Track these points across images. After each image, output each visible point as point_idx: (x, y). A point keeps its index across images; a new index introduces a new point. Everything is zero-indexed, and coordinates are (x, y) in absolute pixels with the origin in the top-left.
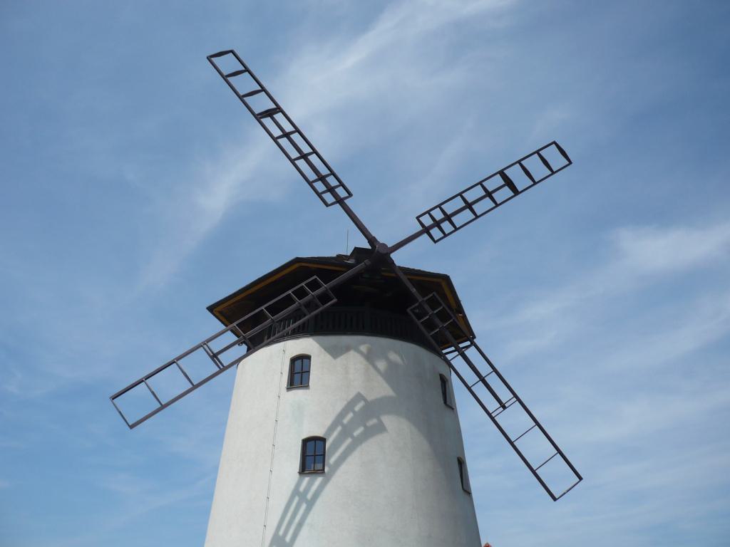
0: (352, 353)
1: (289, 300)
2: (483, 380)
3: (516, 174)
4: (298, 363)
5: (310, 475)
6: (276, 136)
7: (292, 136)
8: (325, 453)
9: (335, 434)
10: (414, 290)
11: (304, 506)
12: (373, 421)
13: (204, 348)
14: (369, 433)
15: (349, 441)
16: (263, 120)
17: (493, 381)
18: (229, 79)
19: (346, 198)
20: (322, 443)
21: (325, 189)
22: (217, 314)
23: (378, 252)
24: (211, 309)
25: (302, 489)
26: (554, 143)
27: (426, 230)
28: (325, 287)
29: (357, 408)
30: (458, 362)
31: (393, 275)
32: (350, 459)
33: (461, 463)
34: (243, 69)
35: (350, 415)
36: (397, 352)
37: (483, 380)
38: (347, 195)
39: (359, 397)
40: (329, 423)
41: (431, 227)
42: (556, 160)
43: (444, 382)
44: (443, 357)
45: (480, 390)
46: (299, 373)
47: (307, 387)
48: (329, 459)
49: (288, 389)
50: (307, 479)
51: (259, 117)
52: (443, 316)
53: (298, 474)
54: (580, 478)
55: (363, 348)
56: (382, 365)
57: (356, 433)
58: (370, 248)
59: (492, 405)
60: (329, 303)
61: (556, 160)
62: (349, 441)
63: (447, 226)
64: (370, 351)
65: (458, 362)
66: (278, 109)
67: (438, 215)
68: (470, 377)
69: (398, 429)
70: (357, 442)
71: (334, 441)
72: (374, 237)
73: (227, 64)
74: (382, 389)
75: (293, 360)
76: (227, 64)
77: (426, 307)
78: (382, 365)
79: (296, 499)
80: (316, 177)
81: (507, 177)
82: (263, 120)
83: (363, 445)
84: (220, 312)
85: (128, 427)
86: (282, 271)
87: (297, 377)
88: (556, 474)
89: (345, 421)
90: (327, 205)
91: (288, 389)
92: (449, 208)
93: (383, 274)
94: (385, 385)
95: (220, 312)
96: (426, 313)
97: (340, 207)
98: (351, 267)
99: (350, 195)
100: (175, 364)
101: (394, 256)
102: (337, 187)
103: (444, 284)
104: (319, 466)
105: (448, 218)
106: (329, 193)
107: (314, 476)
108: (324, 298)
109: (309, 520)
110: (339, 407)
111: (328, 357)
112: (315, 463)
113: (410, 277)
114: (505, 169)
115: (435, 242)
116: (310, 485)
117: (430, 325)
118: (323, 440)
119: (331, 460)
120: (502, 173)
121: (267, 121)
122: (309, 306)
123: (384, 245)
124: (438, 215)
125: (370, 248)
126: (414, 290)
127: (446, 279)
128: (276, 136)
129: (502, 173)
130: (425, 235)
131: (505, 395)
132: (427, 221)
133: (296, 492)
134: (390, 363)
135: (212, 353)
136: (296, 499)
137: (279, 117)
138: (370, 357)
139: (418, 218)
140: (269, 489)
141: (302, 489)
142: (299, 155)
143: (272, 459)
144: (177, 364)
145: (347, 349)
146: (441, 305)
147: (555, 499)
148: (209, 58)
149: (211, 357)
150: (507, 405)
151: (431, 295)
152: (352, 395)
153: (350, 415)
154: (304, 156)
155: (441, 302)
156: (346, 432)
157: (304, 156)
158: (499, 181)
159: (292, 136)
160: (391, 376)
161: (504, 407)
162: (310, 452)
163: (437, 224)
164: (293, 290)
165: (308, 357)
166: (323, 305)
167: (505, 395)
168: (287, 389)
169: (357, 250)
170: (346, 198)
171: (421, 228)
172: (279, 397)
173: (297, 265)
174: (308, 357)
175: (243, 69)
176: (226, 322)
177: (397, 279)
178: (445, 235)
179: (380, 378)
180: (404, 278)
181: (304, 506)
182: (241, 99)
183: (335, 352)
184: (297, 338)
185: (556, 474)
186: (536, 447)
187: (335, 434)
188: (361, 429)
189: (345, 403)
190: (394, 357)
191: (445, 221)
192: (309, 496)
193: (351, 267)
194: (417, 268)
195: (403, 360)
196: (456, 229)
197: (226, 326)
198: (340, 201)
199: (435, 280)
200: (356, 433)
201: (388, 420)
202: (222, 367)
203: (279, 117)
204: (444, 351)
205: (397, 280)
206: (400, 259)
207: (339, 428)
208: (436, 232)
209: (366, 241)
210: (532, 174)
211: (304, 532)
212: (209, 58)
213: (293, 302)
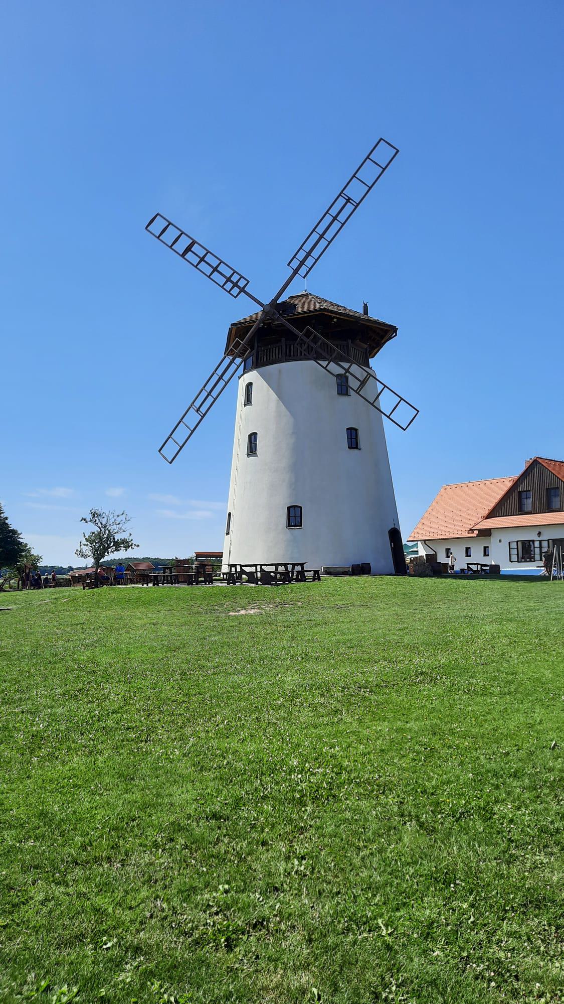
17: (210, 400)
27: (242, 290)
58: (278, 302)
59: (197, 404)
63: (235, 278)
67: (229, 286)
81: (185, 251)
85: (160, 213)
88: (169, 451)
105: (229, 280)
114: (179, 254)
120: (183, 255)
124: (229, 286)
125: (278, 302)
129: (183, 255)
131: (204, 410)
132: (236, 291)
135: (360, 386)
158: (189, 255)
161: (349, 199)
163: (235, 285)
167: (204, 410)
185: (169, 451)
186: (181, 434)
196: (235, 272)
198: (296, 272)
208: (242, 283)
210: (164, 227)
213: (324, 343)
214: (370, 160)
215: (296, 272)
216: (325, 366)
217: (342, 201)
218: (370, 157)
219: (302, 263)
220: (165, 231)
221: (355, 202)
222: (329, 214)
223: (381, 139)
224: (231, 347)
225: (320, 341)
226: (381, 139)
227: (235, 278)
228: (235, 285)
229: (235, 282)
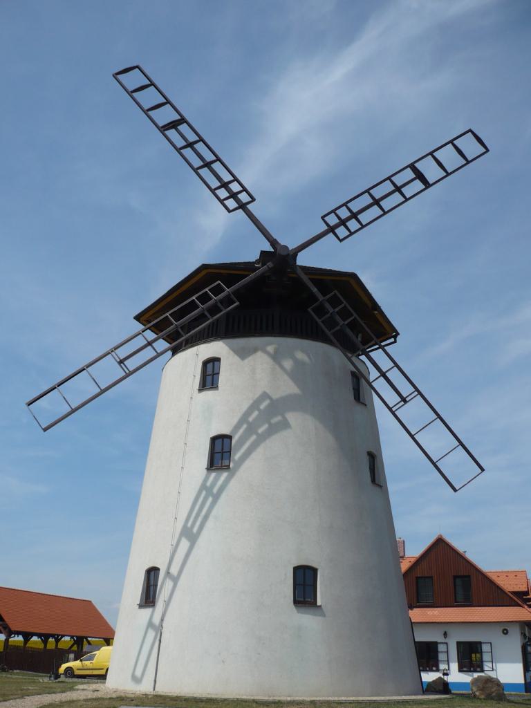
0: (259, 354)
1: (193, 306)
2: (383, 375)
4: (210, 366)
5: (216, 471)
6: (222, 197)
7: (213, 166)
8: (231, 449)
9: (241, 431)
10: (315, 290)
11: (210, 499)
12: (275, 420)
14: (272, 430)
15: (254, 437)
16: (167, 132)
17: (394, 375)
18: (150, 113)
20: (229, 440)
25: (208, 484)
26: (470, 131)
27: (332, 229)
29: (262, 407)
31: (294, 275)
32: (254, 455)
34: (165, 101)
35: (256, 413)
36: (303, 351)
37: (383, 375)
38: (250, 199)
39: (265, 396)
40: (235, 421)
41: (337, 226)
42: (470, 147)
46: (209, 376)
47: (217, 388)
48: (235, 454)
49: (200, 390)
50: (213, 475)
51: (164, 129)
53: (205, 471)
55: (270, 349)
56: (288, 364)
57: (260, 431)
58: (272, 250)
60: (232, 307)
61: (470, 147)
62: (254, 437)
64: (276, 351)
66: (183, 120)
69: (301, 424)
70: (262, 438)
71: (241, 437)
72: (276, 240)
73: (133, 80)
74: (287, 387)
75: (205, 363)
76: (133, 80)
78: (288, 364)
79: (204, 493)
83: (267, 441)
86: (193, 277)
87: (209, 379)
88: (51, 406)
89: (251, 419)
90: (229, 211)
91: (200, 390)
92: (355, 207)
94: (291, 383)
96: (337, 324)
97: (225, 191)
99: (253, 200)
103: (352, 282)
104: (226, 462)
106: (241, 210)
107: (219, 471)
108: (228, 301)
109: (214, 512)
110: (245, 406)
111: (236, 358)
112: (222, 459)
116: (216, 480)
118: (230, 437)
119: (237, 456)
120: (412, 167)
121: (172, 133)
122: (214, 310)
123: (286, 247)
125: (272, 250)
126: (315, 290)
127: (354, 276)
128: (222, 197)
129: (412, 167)
130: (331, 234)
131: (406, 390)
133: (203, 486)
134: (296, 361)
136: (204, 493)
137: (183, 128)
138: (276, 357)
139: (323, 218)
140: (180, 484)
141: (208, 484)
142: (220, 184)
145: (255, 350)
146: (352, 315)
149: (118, 362)
150: (407, 399)
151: (333, 293)
152: (258, 393)
153: (256, 413)
155: (352, 311)
156: (251, 429)
158: (409, 174)
159: (213, 166)
160: (297, 375)
162: (218, 448)
163: (343, 223)
164: (170, 312)
165: (218, 360)
166: (225, 308)
167: (406, 390)
168: (199, 390)
171: (326, 228)
173: (204, 272)
174: (218, 360)
176: (157, 332)
179: (286, 377)
180: (305, 278)
181: (210, 499)
182: (178, 152)
183: (243, 354)
184: (209, 342)
185: (51, 406)
187: (241, 431)
188: (266, 426)
189: (251, 402)
190: (300, 356)
192: (215, 490)
195: (309, 357)
196: (363, 226)
198: (242, 206)
199: (343, 279)
200: (260, 431)
201: (293, 418)
202: (127, 372)
205: (298, 282)
206: (303, 260)
207: (245, 426)
208: (341, 232)
209: (269, 244)
211: (210, 524)
216: (360, 226)
217: (131, 364)
218: (155, 354)
220: (479, 142)
221: (127, 368)
222: (156, 351)
224: (355, 315)
225: (343, 305)
227: (353, 225)
228: (343, 223)
229: (381, 203)
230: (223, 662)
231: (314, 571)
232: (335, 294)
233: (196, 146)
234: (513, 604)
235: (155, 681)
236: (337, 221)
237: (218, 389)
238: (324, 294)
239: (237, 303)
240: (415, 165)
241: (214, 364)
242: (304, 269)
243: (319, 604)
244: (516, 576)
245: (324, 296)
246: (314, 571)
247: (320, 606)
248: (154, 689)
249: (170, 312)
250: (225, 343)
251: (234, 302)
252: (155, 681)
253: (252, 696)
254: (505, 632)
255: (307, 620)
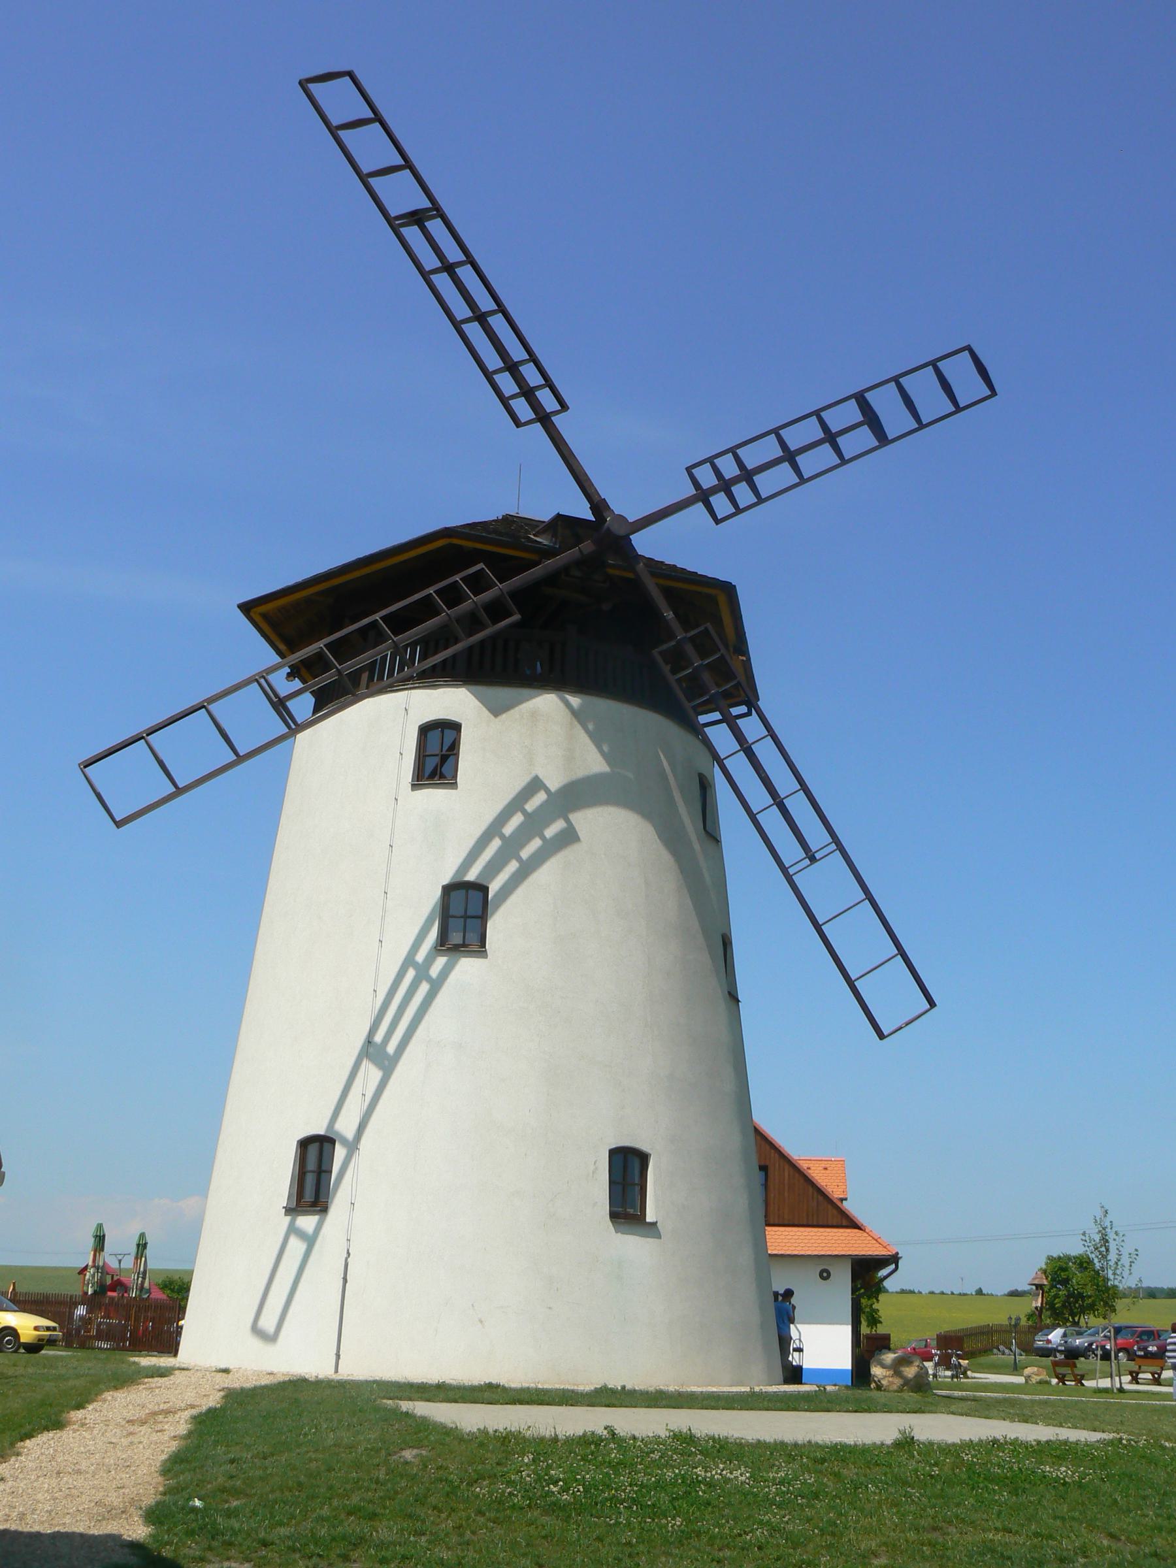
1: (427, 609)
3: (886, 404)
10: (669, 615)
13: (260, 685)
16: (405, 231)
17: (798, 806)
19: (556, 413)
21: (439, 264)
22: (257, 618)
23: (608, 529)
24: (246, 608)
26: (969, 348)
27: (703, 496)
28: (499, 589)
30: (720, 736)
31: (631, 576)
33: (726, 943)
41: (714, 490)
42: (968, 385)
43: (705, 787)
44: (697, 731)
45: (772, 821)
52: (704, 646)
54: (932, 1004)
58: (594, 520)
59: (790, 851)
61: (968, 385)
65: (720, 736)
66: (437, 211)
67: (729, 468)
68: (758, 797)
74: (593, 762)
75: (426, 730)
77: (689, 649)
80: (469, 314)
82: (405, 231)
84: (265, 616)
89: (530, 806)
90: (518, 423)
93: (611, 571)
95: (265, 616)
98: (548, 553)
99: (564, 406)
100: (143, 740)
101: (636, 539)
102: (493, 313)
103: (722, 599)
105: (747, 476)
108: (496, 610)
113: (662, 582)
115: (717, 521)
117: (677, 659)
120: (860, 398)
122: (473, 622)
125: (594, 520)
126: (669, 615)
128: (428, 267)
129: (860, 398)
130: (700, 506)
131: (816, 836)
132: (707, 478)
135: (276, 695)
139: (689, 470)
142: (440, 265)
143: (383, 918)
144: (147, 742)
147: (881, 1036)
148: (303, 84)
150: (818, 856)
154: (449, 268)
157: (449, 268)
158: (851, 413)
161: (813, 859)
162: (457, 908)
163: (725, 486)
164: (384, 612)
165: (456, 727)
167: (816, 836)
168: (412, 785)
169: (561, 521)
170: (556, 413)
172: (396, 799)
174: (456, 727)
175: (402, 162)
176: (282, 647)
177: (635, 585)
178: (739, 511)
180: (651, 585)
191: (740, 481)
193: (548, 553)
194: (669, 561)
196: (760, 500)
197: (281, 655)
198: (544, 419)
203: (435, 226)
204: (703, 719)
208: (720, 502)
212: (303, 84)
214: (803, 857)
215: (544, 419)
219: (528, 393)
223: (118, 824)
226: (118, 824)
228: (725, 486)
230: (481, 1321)
231: (643, 1158)
232: (706, 629)
233: (459, 271)
234: (844, 1223)
235: (338, 1356)
236: (714, 481)
237: (456, 788)
238: (687, 625)
239: (516, 617)
240: (866, 395)
241: (442, 732)
242: (657, 568)
243: (650, 1218)
244: (826, 1169)
245: (686, 631)
246: (643, 1158)
247: (654, 1224)
248: (336, 1371)
249: (384, 612)
250: (468, 690)
251: (510, 615)
252: (338, 1356)
253: (574, 1385)
254: (825, 1275)
255: (631, 1245)
